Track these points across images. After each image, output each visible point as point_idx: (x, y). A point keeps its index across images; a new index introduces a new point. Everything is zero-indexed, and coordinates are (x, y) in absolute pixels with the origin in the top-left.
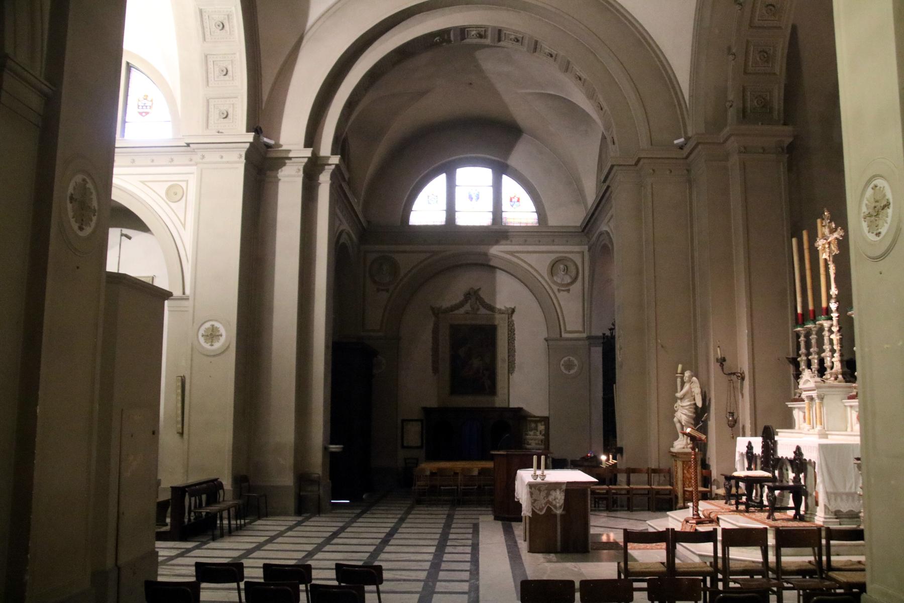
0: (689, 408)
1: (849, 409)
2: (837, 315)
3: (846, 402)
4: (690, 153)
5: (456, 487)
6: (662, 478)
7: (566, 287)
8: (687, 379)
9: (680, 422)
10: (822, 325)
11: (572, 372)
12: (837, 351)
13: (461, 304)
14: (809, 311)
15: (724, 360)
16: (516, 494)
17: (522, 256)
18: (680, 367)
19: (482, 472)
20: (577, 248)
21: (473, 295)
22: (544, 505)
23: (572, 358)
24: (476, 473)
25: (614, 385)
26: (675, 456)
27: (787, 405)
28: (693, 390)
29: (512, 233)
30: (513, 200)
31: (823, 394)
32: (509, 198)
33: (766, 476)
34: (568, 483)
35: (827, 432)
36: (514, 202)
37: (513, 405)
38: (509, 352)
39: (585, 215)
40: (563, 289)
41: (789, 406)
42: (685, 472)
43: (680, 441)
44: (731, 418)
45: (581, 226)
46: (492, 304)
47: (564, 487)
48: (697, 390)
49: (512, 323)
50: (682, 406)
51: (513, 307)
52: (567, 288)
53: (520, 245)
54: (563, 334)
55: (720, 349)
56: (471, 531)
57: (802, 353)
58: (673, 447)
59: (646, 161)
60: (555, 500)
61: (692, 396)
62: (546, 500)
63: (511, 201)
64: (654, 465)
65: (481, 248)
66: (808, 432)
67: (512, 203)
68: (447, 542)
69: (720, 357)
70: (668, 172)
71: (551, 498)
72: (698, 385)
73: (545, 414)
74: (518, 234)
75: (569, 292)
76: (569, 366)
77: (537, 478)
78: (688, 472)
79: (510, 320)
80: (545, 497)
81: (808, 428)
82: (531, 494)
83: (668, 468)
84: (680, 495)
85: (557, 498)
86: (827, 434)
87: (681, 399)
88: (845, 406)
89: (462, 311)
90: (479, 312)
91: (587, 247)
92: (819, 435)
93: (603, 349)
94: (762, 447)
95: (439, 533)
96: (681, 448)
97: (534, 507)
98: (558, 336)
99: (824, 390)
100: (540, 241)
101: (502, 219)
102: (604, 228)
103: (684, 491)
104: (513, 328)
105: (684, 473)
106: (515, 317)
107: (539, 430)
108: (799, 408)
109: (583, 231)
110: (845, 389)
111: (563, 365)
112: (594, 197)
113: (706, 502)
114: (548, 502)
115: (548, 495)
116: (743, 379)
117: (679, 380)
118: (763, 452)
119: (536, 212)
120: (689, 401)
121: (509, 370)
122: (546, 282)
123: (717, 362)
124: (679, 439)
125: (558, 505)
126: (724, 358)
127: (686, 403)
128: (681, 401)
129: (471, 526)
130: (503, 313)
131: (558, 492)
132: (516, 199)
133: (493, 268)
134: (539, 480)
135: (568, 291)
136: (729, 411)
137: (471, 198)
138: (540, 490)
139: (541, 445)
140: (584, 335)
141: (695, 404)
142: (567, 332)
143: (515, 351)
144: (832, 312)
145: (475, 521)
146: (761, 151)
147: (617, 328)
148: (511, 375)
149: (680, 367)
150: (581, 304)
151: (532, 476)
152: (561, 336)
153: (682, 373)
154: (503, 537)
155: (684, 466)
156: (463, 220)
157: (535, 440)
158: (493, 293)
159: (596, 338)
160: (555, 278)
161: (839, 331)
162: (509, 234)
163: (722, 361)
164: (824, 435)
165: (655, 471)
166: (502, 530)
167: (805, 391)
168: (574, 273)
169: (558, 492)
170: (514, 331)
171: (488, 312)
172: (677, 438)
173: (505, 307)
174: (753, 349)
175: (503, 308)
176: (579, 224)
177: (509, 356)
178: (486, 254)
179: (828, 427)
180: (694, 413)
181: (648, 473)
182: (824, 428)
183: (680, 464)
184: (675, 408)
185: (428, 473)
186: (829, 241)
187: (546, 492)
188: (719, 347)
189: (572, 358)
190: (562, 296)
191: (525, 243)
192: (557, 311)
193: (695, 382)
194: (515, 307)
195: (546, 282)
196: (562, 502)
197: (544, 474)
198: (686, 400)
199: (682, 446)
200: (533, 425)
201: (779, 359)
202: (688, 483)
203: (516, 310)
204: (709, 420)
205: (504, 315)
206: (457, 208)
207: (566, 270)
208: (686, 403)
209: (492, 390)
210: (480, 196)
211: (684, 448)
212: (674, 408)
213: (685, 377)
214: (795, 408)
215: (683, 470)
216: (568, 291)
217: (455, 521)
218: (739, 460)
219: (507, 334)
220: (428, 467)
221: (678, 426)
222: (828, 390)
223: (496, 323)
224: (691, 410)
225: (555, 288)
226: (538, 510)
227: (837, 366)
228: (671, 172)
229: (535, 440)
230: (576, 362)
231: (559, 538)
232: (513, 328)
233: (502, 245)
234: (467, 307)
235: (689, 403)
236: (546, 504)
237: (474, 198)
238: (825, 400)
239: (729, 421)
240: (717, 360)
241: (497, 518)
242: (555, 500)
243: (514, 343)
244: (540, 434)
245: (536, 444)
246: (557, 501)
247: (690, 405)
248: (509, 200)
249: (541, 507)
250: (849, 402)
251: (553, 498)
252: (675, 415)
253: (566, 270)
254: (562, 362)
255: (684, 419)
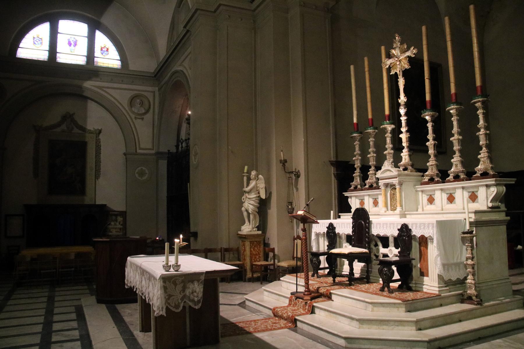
0: (255, 200)
1: (420, 193)
2: (406, 118)
3: (419, 188)
4: (258, 6)
5: (54, 270)
6: (232, 255)
7: (141, 116)
8: (253, 177)
9: (247, 211)
10: (385, 129)
11: (144, 178)
12: (405, 147)
13: (59, 125)
14: (369, 119)
15: (285, 161)
16: (126, 281)
17: (107, 90)
18: (246, 168)
19: (79, 255)
20: (150, 89)
21: (68, 118)
22: (180, 301)
23: (144, 168)
24: (72, 257)
25: (188, 184)
26: (244, 238)
27: (344, 195)
28: (258, 185)
29: (101, 73)
30: (103, 49)
31: (403, 181)
32: (100, 48)
33: (364, 251)
34: (207, 272)
35: (406, 213)
36: (104, 51)
37: (98, 202)
38: (96, 163)
39: (157, 66)
40: (139, 117)
41: (345, 195)
42: (252, 250)
43: (246, 226)
44: (290, 207)
45: (154, 73)
46: (84, 126)
47: (203, 278)
48: (262, 185)
49: (99, 141)
50: (249, 198)
51: (100, 129)
52: (142, 117)
53: (107, 82)
54: (138, 149)
55: (283, 153)
56: (74, 316)
57: (358, 154)
58: (240, 230)
59: (224, 8)
60: (192, 293)
61: (257, 190)
62: (183, 294)
63: (102, 50)
64: (225, 246)
65: (77, 82)
66: (385, 213)
67: (102, 52)
68: (51, 337)
69: (283, 159)
70: (240, 20)
71: (188, 292)
72: (263, 181)
73: (122, 208)
74: (107, 73)
75: (143, 120)
76: (142, 174)
77: (170, 269)
78: (254, 250)
79: (98, 138)
80: (181, 291)
81: (385, 210)
82: (165, 288)
83: (237, 247)
84: (248, 267)
85: (195, 292)
86: (405, 214)
87: (249, 192)
88: (416, 191)
89: (58, 130)
90: (73, 132)
91: (157, 88)
92: (400, 215)
93: (168, 162)
94: (353, 227)
95: (41, 323)
96: (248, 231)
97: (169, 304)
98: (134, 152)
99: (403, 177)
100: (122, 81)
101: (94, 62)
102: (177, 67)
103: (252, 265)
104: (99, 144)
105: (251, 251)
106: (101, 137)
107: (118, 221)
108: (356, 196)
109: (155, 76)
110: (416, 177)
111: (137, 173)
112: (165, 54)
113: (292, 275)
114: (184, 297)
115: (184, 289)
116: (298, 176)
117: (245, 179)
118: (353, 232)
119: (120, 60)
120: (255, 194)
121: (95, 175)
122: (126, 111)
123: (281, 163)
124: (246, 224)
125: (196, 299)
126: (286, 160)
127: (253, 196)
128: (248, 195)
129: (73, 309)
130: (92, 133)
131: (196, 284)
132: (105, 49)
133: (86, 98)
134: (172, 271)
135: (143, 119)
136: (288, 201)
137: (70, 44)
138: (175, 284)
139: (120, 232)
140: (153, 152)
141: (259, 196)
142: (140, 149)
143: (100, 162)
144: (401, 116)
145: (76, 303)
146: (314, 7)
147: (191, 138)
148: (98, 180)
149: (246, 168)
150: (151, 130)
151: (164, 266)
152: (136, 152)
153: (249, 172)
154: (116, 329)
155: (251, 245)
156: (62, 58)
157: (115, 229)
158: (85, 118)
159: (161, 153)
160: (133, 109)
161: (407, 131)
162: (100, 73)
163: (284, 162)
164: (403, 215)
165: (227, 250)
166: (111, 318)
167: (381, 180)
168: (147, 107)
169: (196, 284)
170: (101, 147)
171: (80, 132)
172: (243, 223)
173: (94, 128)
174: (307, 155)
175: (92, 129)
176: (153, 71)
177: (96, 166)
178: (80, 87)
179: (405, 208)
180: (259, 203)
181: (221, 251)
182: (403, 210)
183: (247, 244)
184: (242, 200)
185: (29, 259)
186: (400, 59)
187: (182, 285)
188: (282, 151)
189: (144, 168)
190: (138, 122)
191: (112, 81)
192: (133, 134)
193: (261, 179)
194: (101, 129)
195: (126, 111)
196: (201, 295)
197: (179, 264)
198: (253, 194)
199: (250, 230)
200: (114, 217)
201: (324, 162)
202: (254, 258)
203: (102, 131)
204: (270, 209)
205: (92, 135)
206: (58, 50)
207: (142, 104)
208: (253, 196)
209: (83, 192)
210: (78, 43)
211: (251, 231)
212: (242, 200)
213: (251, 176)
214: (351, 197)
215: (251, 248)
216: (143, 119)
217: (56, 304)
218: (315, 239)
219: (94, 149)
220: (28, 253)
221: (245, 214)
222: (404, 177)
223: (87, 140)
224: (256, 201)
225: (133, 116)
226: (174, 307)
227: (405, 159)
228: (242, 20)
229: (115, 229)
230: (147, 171)
231: (188, 330)
232: (99, 144)
233: (93, 81)
234: (64, 127)
235: (255, 196)
236: (182, 299)
237: (73, 44)
238: (403, 186)
239: (289, 209)
240: (281, 161)
241: (99, 301)
242: (192, 293)
243: (100, 156)
244: (119, 224)
245: (116, 232)
246: (195, 294)
247: (257, 197)
248: (100, 49)
249: (177, 303)
250: (421, 188)
251: (191, 291)
252: (243, 205)
253: (141, 104)
254: (137, 171)
255: (251, 208)
